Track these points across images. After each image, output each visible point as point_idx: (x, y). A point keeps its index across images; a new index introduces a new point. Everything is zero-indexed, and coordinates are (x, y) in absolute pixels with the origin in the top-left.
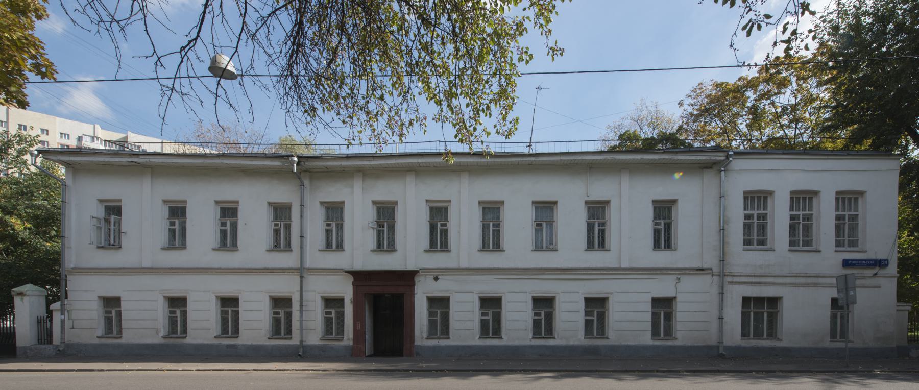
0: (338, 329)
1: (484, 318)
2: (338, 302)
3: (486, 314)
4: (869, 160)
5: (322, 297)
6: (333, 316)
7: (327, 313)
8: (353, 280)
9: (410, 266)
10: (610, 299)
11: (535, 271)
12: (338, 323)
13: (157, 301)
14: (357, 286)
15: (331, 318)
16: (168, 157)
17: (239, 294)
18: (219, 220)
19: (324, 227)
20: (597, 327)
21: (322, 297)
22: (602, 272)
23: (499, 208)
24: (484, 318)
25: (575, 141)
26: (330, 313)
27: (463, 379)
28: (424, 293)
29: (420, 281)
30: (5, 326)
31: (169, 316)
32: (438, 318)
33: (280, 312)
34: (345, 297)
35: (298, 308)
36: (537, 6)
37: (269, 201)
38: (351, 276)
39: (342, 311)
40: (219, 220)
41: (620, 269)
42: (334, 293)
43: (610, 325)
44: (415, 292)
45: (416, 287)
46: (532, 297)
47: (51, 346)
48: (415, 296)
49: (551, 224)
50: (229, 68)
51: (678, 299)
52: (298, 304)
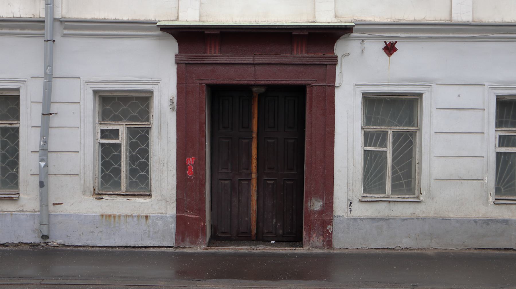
0: (132, 172)
1: (504, 150)
3: (381, 139)
5: (95, 92)
6: (123, 140)
7: (105, 134)
8: (177, 51)
11: (32, 28)
12: (132, 159)
13: (80, 103)
17: (154, 89)
20: (7, 155)
21: (95, 92)
24: (504, 150)
26: (115, 134)
27: (253, 282)
28: (357, 85)
29: (348, 55)
31: (102, 145)
33: (118, 131)
35: (37, 119)
38: (335, 45)
39: (142, 130)
42: (370, 91)
43: (425, 166)
44: (337, 84)
45: (338, 69)
46: (363, 94)
48: (336, 91)
52: (38, 110)
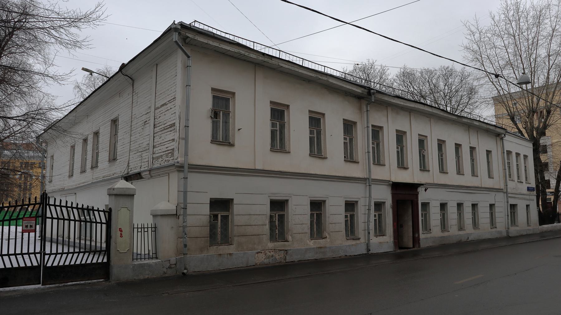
2: (379, 206)
4: (524, 141)
9: (416, 182)
10: (448, 203)
14: (394, 194)
15: (348, 220)
16: (291, 63)
18: (321, 130)
19: (396, 150)
22: (478, 189)
23: (228, 100)
25: (293, 56)
30: (88, 243)
32: (349, 219)
34: (137, 193)
36: (468, 43)
37: (346, 118)
38: (418, 188)
40: (230, 112)
41: (481, 188)
47: (184, 269)
49: (227, 114)
50: (512, 91)
51: (496, 205)
